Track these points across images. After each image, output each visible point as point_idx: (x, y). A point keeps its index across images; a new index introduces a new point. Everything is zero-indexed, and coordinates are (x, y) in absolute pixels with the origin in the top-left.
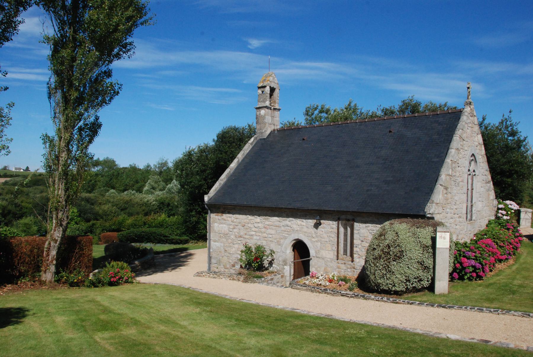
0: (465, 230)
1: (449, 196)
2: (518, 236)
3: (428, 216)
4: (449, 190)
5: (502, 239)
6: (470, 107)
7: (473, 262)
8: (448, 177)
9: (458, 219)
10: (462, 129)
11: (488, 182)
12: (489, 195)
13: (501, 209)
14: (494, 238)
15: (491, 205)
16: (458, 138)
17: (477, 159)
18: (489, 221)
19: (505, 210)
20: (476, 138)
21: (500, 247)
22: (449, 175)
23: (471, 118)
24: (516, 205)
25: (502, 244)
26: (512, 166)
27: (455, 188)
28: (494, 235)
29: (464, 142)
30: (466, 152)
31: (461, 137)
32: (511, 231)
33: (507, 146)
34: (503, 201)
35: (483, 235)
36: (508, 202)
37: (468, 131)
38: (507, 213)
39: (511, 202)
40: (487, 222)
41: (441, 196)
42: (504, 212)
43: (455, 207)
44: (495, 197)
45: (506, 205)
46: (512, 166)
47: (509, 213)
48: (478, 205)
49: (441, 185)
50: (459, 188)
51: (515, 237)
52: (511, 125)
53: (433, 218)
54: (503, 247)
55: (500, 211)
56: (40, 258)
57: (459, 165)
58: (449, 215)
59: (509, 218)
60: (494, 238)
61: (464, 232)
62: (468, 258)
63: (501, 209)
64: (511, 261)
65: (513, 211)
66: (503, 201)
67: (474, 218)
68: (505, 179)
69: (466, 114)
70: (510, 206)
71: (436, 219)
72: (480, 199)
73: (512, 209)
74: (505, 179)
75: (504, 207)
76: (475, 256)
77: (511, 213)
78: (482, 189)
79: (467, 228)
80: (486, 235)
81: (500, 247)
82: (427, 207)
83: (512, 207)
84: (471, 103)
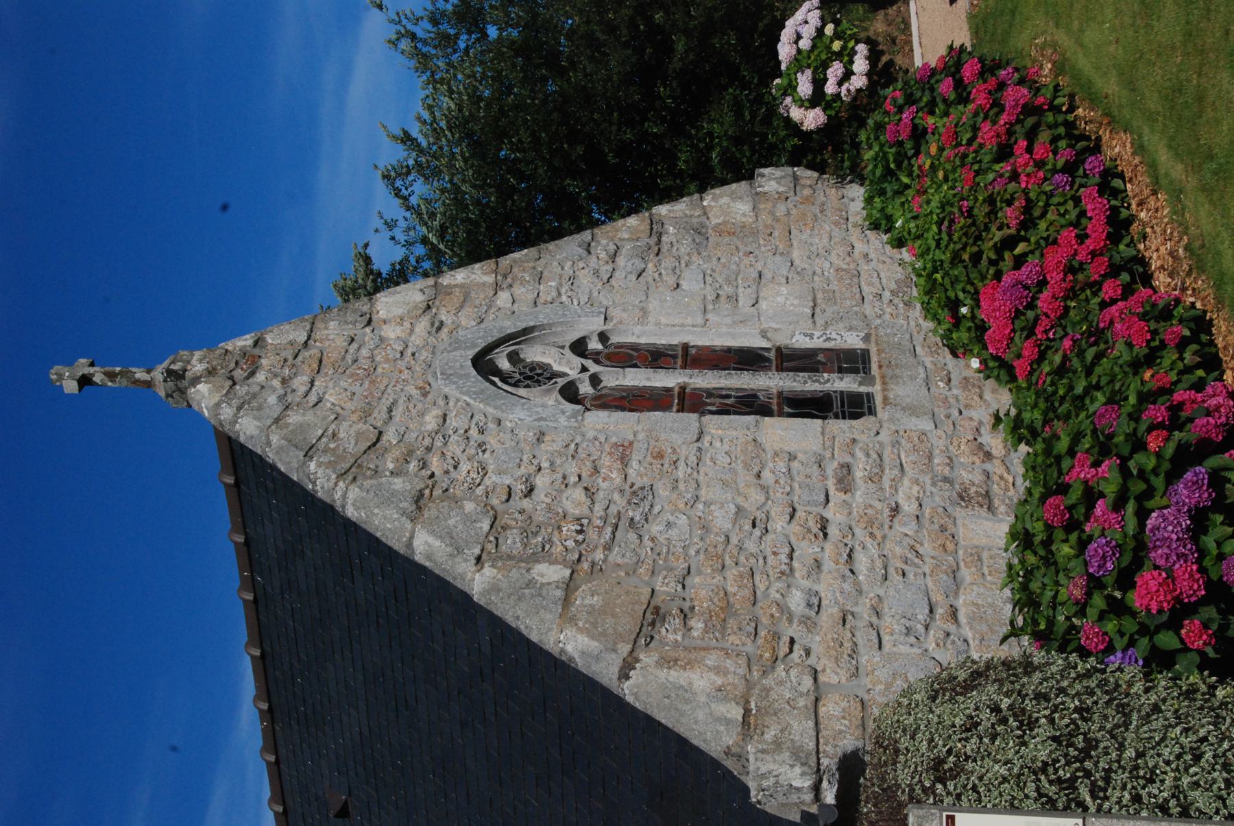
0: (926, 425)
1: (702, 588)
2: (959, 85)
3: (830, 798)
4: (666, 587)
5: (981, 212)
6: (196, 381)
7: (1166, 523)
8: (585, 598)
9: (859, 497)
10: (308, 455)
11: (656, 230)
12: (729, 231)
13: (819, 83)
14: (976, 258)
15: (781, 209)
16: (354, 493)
17: (510, 327)
18: (875, 226)
19: (825, 65)
20: (392, 332)
21: (1028, 223)
22: (569, 587)
23: (260, 377)
24: (799, 16)
25: (1011, 215)
26: (611, 29)
27: (656, 528)
28: (956, 259)
29: (390, 436)
30: (452, 422)
31: (352, 471)
32: (931, 120)
33: (521, 49)
34: (779, 74)
35: (957, 320)
36: (785, 51)
37: (331, 398)
38: (838, 55)
39: (786, 35)
40: (877, 242)
41: (700, 681)
42: (835, 71)
43: (779, 524)
44: (742, 187)
45: (799, 61)
46: (611, 29)
47: (837, 46)
48: (779, 315)
49: (624, 676)
50: (663, 491)
51: (963, 99)
52: (434, 21)
53: (851, 766)
54: (1029, 206)
55: (830, 88)
56: (1040, 749)
57: (519, 487)
58: (829, 587)
59: (862, 49)
60: (976, 258)
61: (938, 441)
62: (1137, 553)
63: (819, 83)
64: (1117, 148)
65: (829, 29)
66: (779, 74)
67: (853, 341)
68: (676, 64)
69: (227, 412)
70: (805, 44)
71: (849, 743)
72: (744, 301)
73: (820, 31)
74: (676, 64)
75: (809, 72)
76: (1119, 504)
77: (837, 35)
78: (690, 283)
79: (913, 410)
80: (954, 305)
81: (1028, 223)
82: (771, 808)
83: (808, 32)
84: (170, 373)
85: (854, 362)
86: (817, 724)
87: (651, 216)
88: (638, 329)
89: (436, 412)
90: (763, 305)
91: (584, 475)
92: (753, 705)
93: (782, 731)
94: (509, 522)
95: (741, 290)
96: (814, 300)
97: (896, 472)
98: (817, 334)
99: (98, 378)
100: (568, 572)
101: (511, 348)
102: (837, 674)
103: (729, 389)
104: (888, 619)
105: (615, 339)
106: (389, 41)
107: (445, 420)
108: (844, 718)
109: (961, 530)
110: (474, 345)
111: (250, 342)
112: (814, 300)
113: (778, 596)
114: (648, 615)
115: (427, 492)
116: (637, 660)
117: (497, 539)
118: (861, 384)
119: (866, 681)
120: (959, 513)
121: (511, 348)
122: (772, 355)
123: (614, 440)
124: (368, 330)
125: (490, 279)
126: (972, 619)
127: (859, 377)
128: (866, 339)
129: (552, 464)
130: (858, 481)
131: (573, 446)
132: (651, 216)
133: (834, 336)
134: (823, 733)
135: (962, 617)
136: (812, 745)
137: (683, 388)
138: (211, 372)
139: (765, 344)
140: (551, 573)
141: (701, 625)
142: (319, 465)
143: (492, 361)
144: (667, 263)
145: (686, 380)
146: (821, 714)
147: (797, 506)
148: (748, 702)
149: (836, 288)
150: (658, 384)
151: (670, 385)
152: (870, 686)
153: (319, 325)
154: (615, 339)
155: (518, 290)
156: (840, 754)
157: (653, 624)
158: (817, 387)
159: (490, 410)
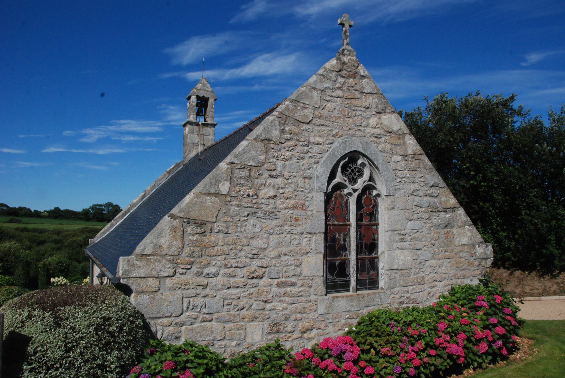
6: (339, 59)
85: (373, 284)
86: (144, 277)
87: (458, 208)
88: (383, 207)
89: (321, 140)
90: (398, 252)
91: (284, 195)
92: (151, 257)
93: (139, 267)
94: (253, 172)
95: (408, 243)
96: (402, 269)
97: (290, 302)
98: (383, 271)
99: (344, 29)
100: (225, 193)
101: (367, 163)
102: (170, 283)
103: (350, 241)
104: (202, 300)
105: (379, 199)
106: (512, 98)
107: (317, 144)
108: (147, 286)
109: (255, 324)
110: (365, 150)
111: (362, 74)
112: (402, 269)
113: (214, 264)
114: (200, 222)
115: (272, 142)
116: (175, 219)
117: (244, 168)
118: (353, 287)
119: (168, 293)
120: (266, 323)
121: (367, 163)
122: (373, 255)
123: (307, 203)
124: (374, 113)
125: (410, 152)
126: (204, 328)
127: (355, 287)
128: (382, 289)
129: (291, 183)
130: (285, 289)
131: (302, 189)
132: (458, 208)
133: (383, 277)
134: (139, 280)
135: (203, 324)
136: (131, 276)
137: (349, 225)
138: (344, 63)
139: (379, 252)
140: (224, 188)
141: (195, 239)
142: (288, 105)
143: (360, 157)
144: (426, 216)
145: (353, 226)
146: (149, 279)
147: (268, 269)
148: (153, 255)
149: (411, 277)
150: (351, 217)
151: (351, 221)
152: (164, 294)
153: (375, 96)
154: (379, 199)
155: (403, 163)
156: (129, 285)
157: (195, 223)
158: (352, 272)
159: (324, 159)
